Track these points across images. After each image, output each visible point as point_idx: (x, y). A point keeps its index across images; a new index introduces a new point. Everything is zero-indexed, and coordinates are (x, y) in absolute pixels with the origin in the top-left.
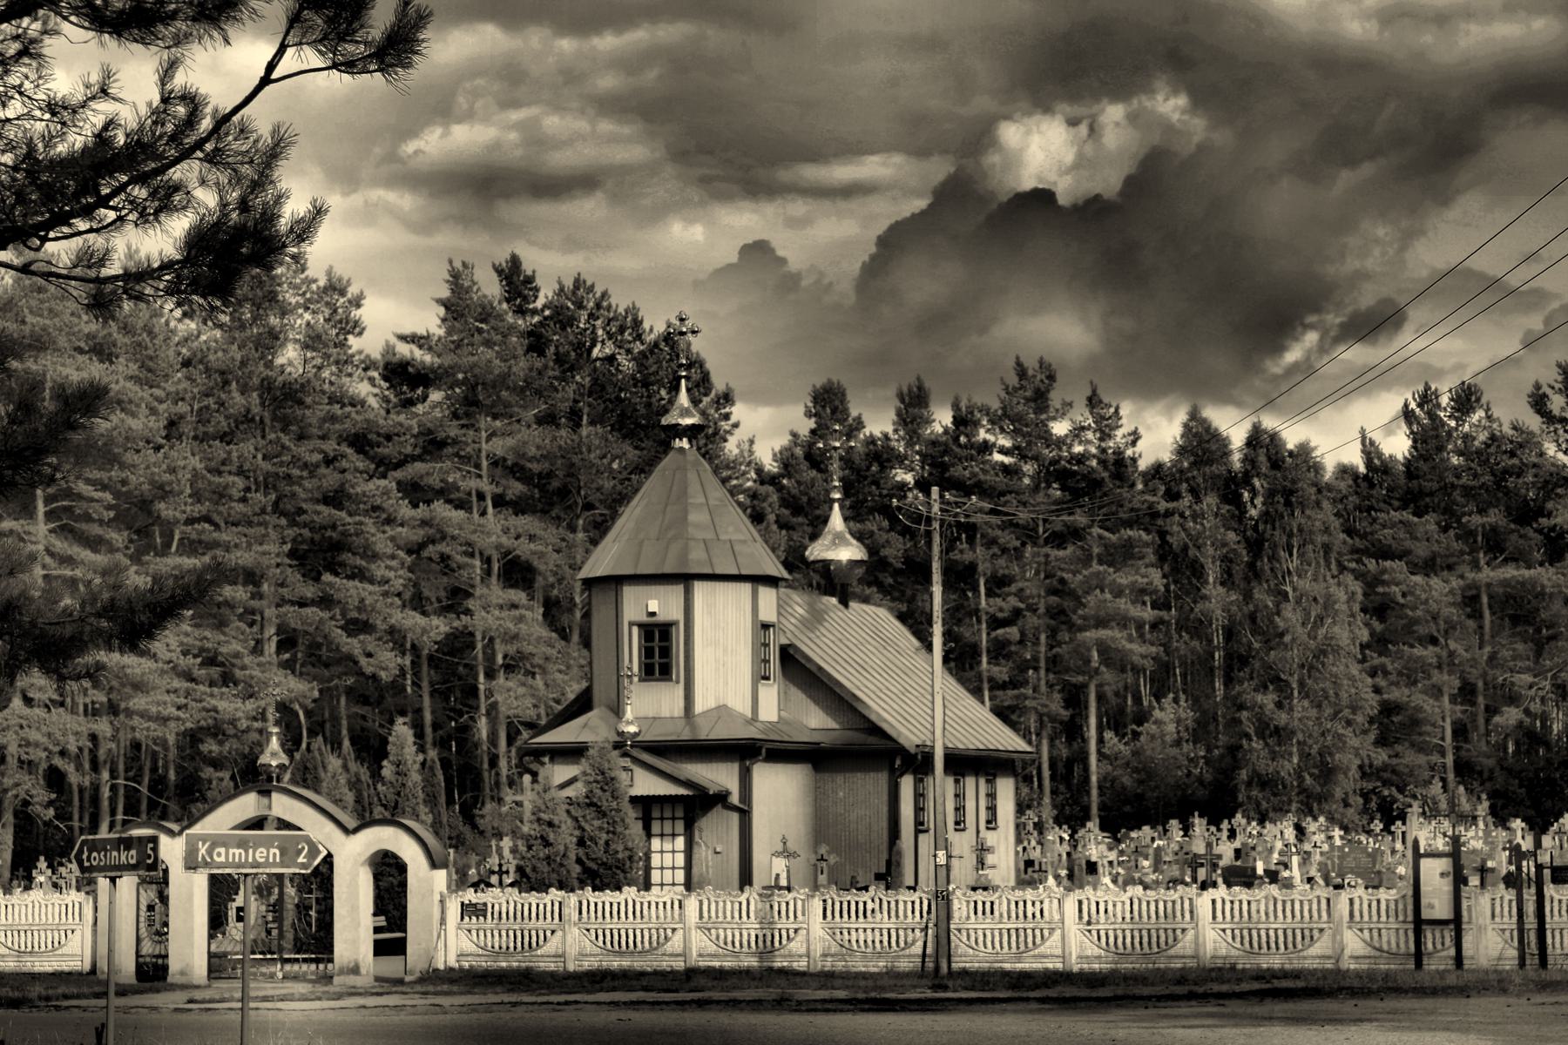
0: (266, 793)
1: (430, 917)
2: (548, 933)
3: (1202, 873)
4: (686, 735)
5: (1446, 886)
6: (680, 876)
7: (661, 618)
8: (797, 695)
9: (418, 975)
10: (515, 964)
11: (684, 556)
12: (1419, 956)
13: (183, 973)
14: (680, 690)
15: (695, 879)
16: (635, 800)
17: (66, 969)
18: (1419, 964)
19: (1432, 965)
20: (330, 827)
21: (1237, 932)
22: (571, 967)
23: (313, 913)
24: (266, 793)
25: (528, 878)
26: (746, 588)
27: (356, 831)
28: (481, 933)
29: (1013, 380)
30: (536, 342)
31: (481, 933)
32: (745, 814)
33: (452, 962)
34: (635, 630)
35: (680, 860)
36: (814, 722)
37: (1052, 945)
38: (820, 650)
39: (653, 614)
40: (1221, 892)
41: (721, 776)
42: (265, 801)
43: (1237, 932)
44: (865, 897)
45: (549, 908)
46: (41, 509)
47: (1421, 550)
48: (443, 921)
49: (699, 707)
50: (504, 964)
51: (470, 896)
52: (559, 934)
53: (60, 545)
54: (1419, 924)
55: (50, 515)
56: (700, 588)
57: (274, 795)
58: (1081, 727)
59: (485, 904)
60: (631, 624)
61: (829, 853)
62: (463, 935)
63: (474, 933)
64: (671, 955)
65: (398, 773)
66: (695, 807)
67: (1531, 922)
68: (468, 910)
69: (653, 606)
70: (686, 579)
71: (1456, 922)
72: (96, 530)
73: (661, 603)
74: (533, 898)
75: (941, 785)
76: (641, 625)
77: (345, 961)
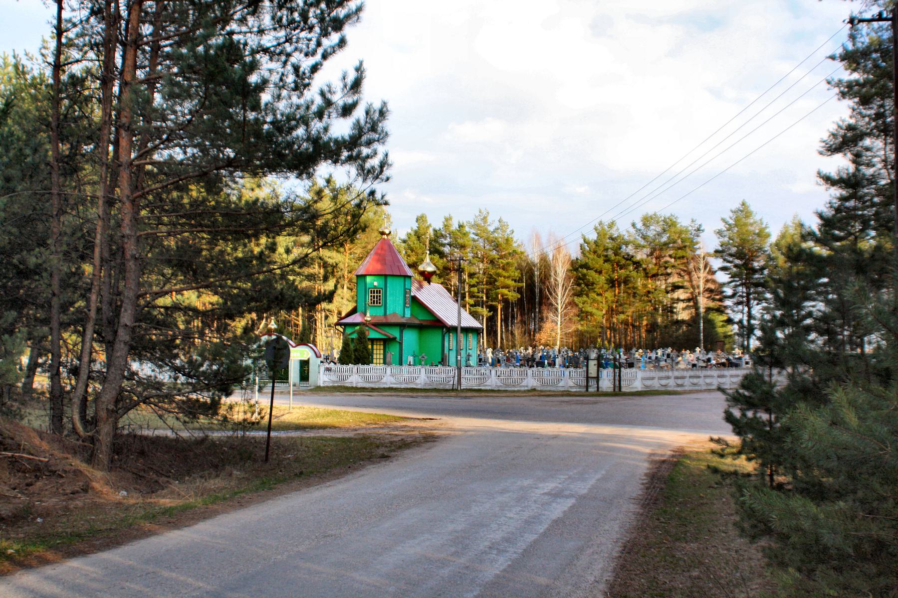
3: (530, 363)
4: (384, 321)
5: (596, 368)
6: (382, 361)
8: (416, 308)
12: (587, 387)
14: (383, 308)
15: (388, 360)
16: (369, 339)
18: (587, 390)
19: (590, 390)
26: (402, 279)
29: (477, 214)
32: (401, 344)
35: (382, 356)
36: (422, 317)
37: (488, 382)
38: (422, 296)
40: (535, 369)
41: (395, 333)
44: (437, 368)
49: (388, 313)
54: (588, 378)
56: (389, 279)
58: (274, 170)
66: (387, 342)
67: (617, 378)
71: (597, 378)
74: (345, 366)
75: (462, 337)
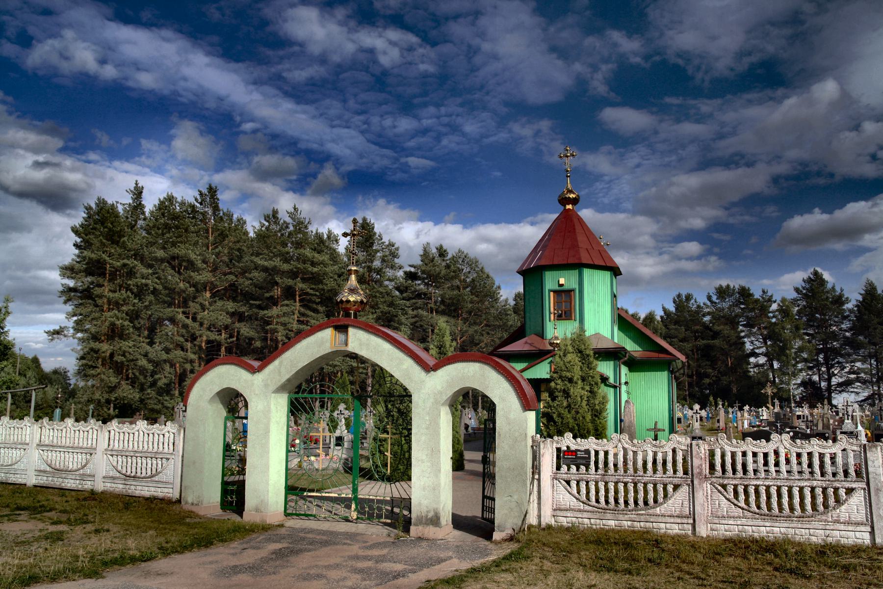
0: (342, 329)
1: (523, 466)
2: (670, 488)
7: (566, 287)
9: (510, 532)
10: (626, 524)
11: (580, 259)
13: (257, 510)
17: (161, 495)
20: (409, 362)
21: (741, 489)
22: (703, 531)
23: (388, 454)
24: (342, 329)
25: (555, 422)
27: (435, 368)
28: (583, 485)
30: (448, 267)
31: (583, 485)
33: (548, 518)
34: (552, 293)
39: (562, 285)
42: (342, 337)
43: (741, 489)
45: (670, 458)
46: (298, 298)
47: (681, 336)
48: (536, 468)
50: (612, 523)
51: (568, 441)
52: (685, 489)
53: (302, 310)
55: (300, 301)
56: (587, 272)
57: (351, 331)
59: (587, 452)
60: (550, 291)
61: (701, 409)
62: (561, 488)
63: (574, 484)
64: (848, 523)
65: (440, 353)
68: (564, 457)
69: (562, 281)
70: (579, 266)
72: (315, 306)
73: (566, 279)
76: (555, 292)
77: (424, 510)
